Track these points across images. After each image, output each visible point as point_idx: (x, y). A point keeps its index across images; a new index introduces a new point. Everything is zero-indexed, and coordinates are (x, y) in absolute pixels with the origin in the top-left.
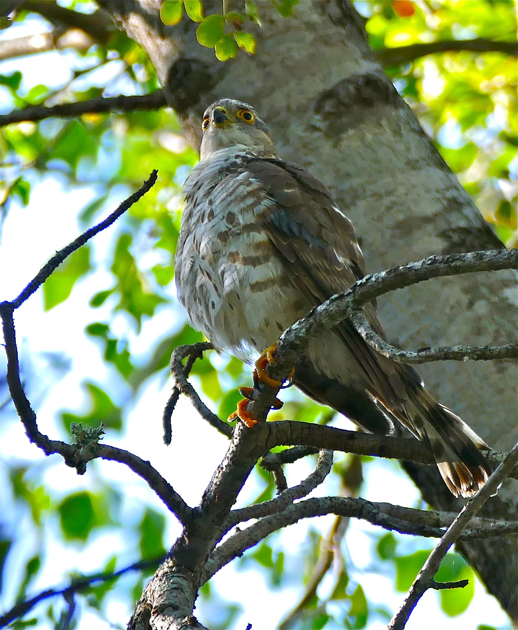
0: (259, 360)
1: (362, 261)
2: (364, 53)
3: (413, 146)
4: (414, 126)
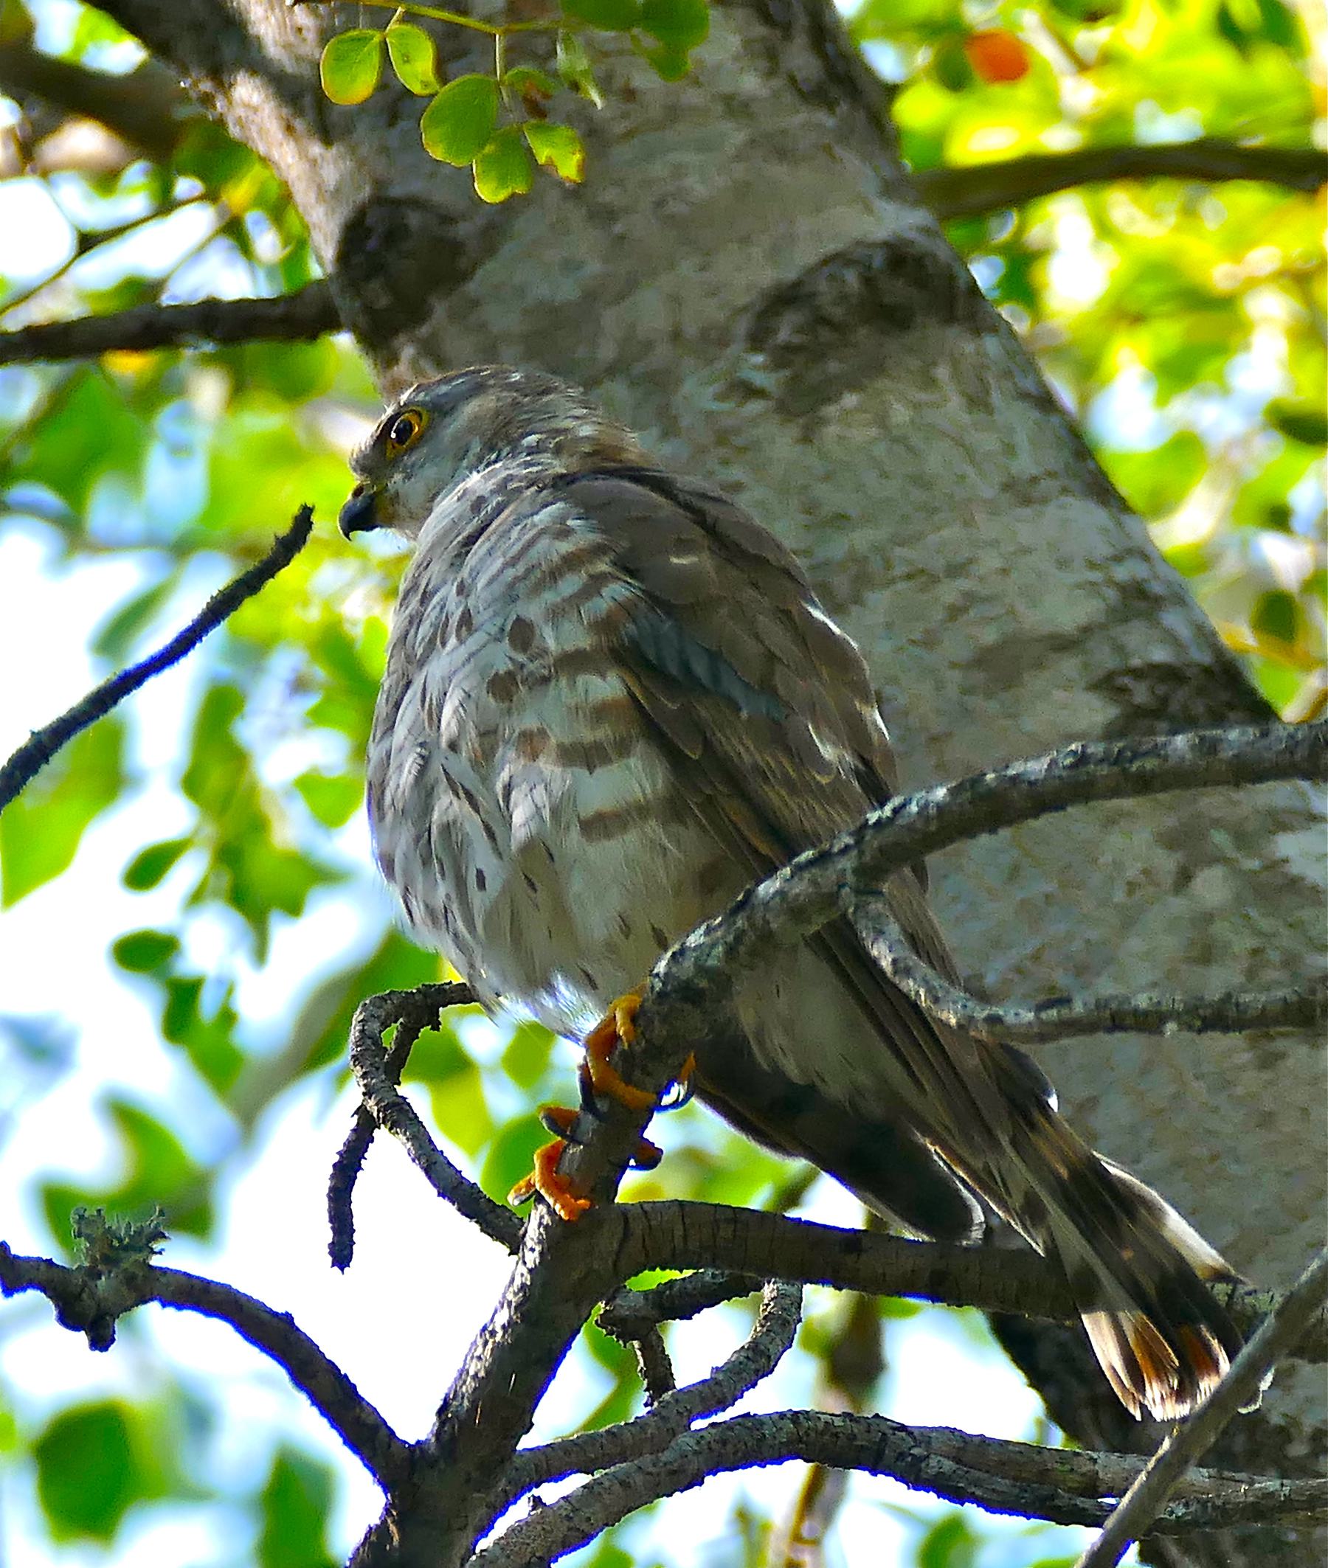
0: (598, 1031)
1: (888, 756)
2: (886, 181)
3: (1022, 439)
4: (1028, 384)
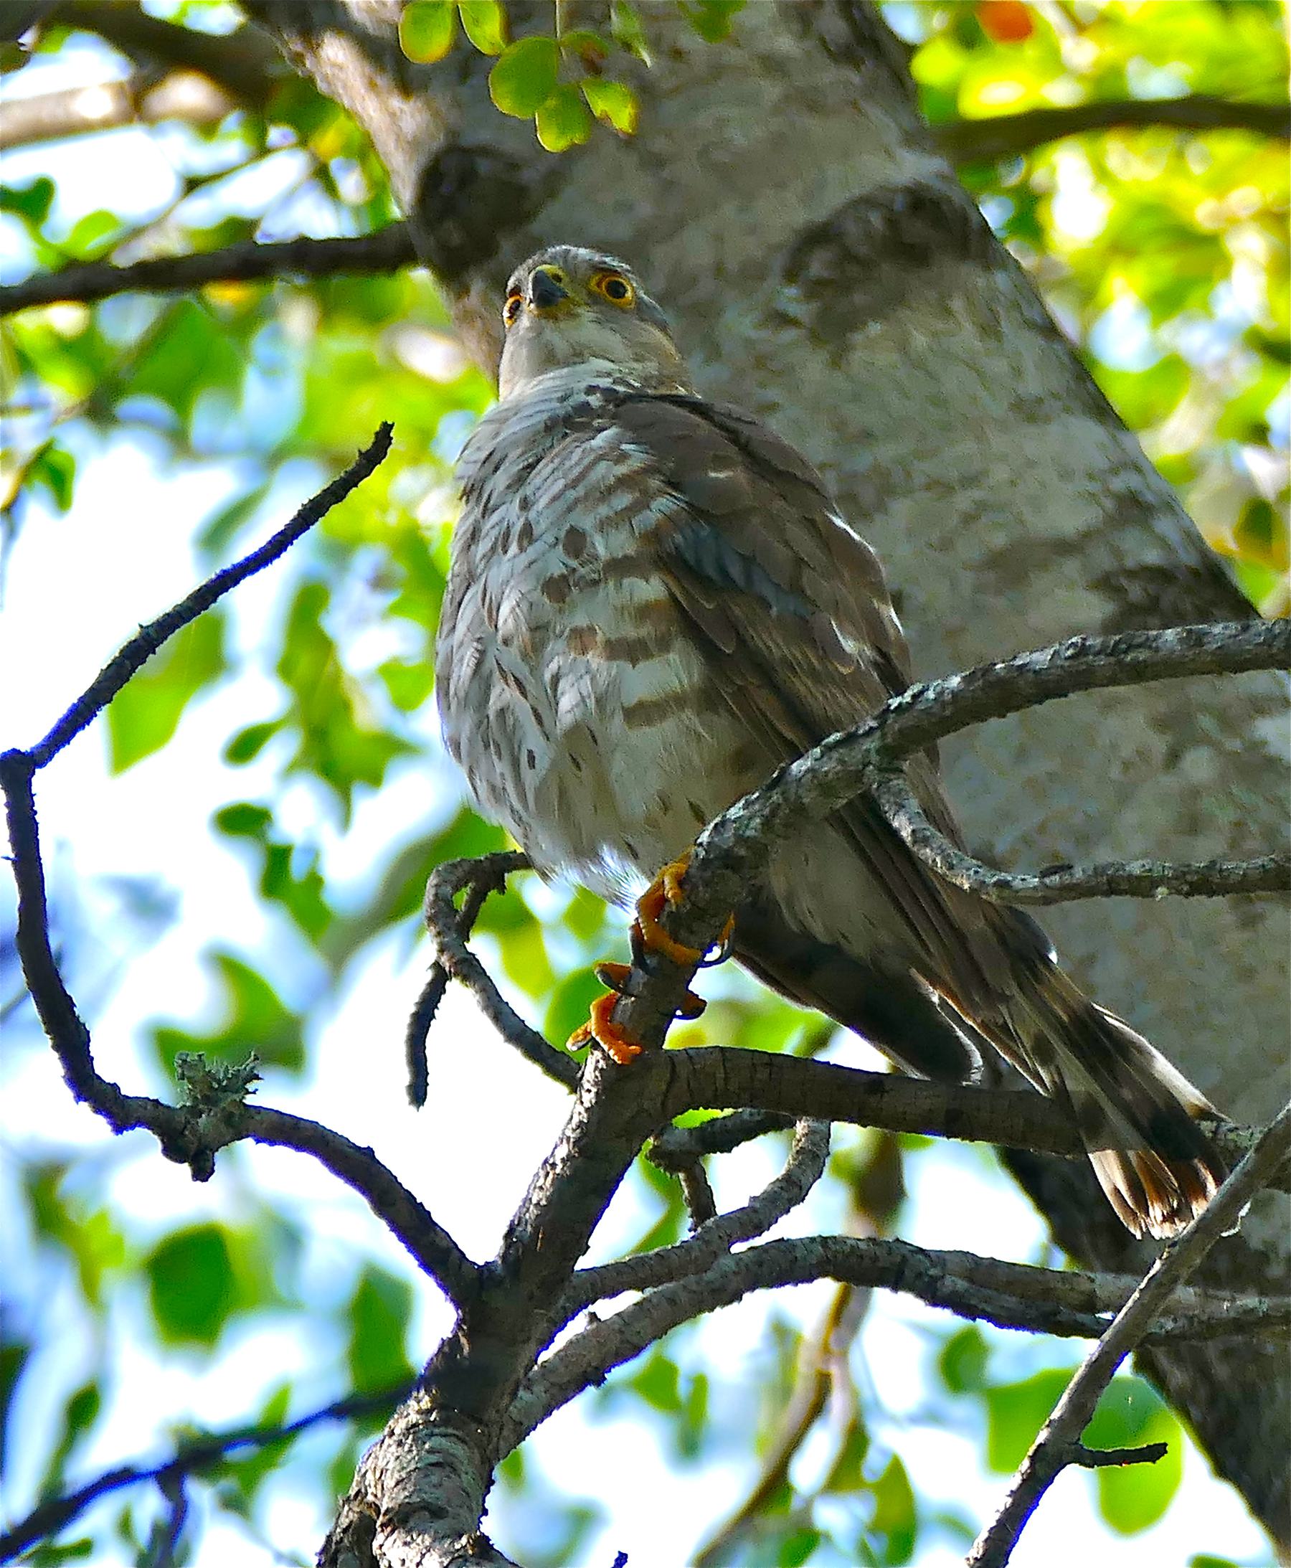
0: (646, 896)
1: (903, 649)
2: (906, 133)
3: (1029, 365)
4: (1033, 314)
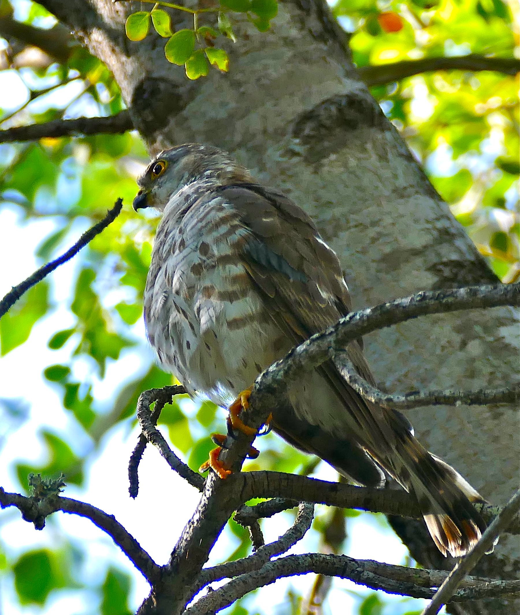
0: (234, 405)
1: (348, 296)
2: (347, 71)
3: (400, 172)
4: (403, 151)
